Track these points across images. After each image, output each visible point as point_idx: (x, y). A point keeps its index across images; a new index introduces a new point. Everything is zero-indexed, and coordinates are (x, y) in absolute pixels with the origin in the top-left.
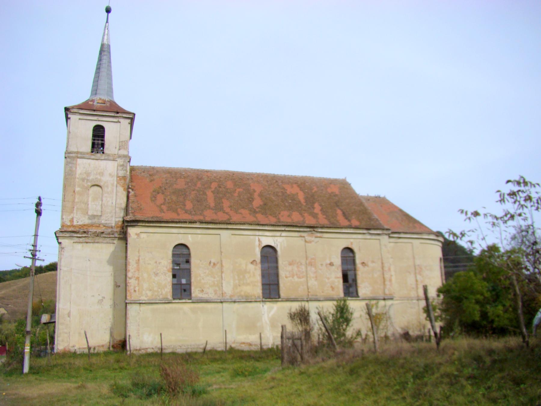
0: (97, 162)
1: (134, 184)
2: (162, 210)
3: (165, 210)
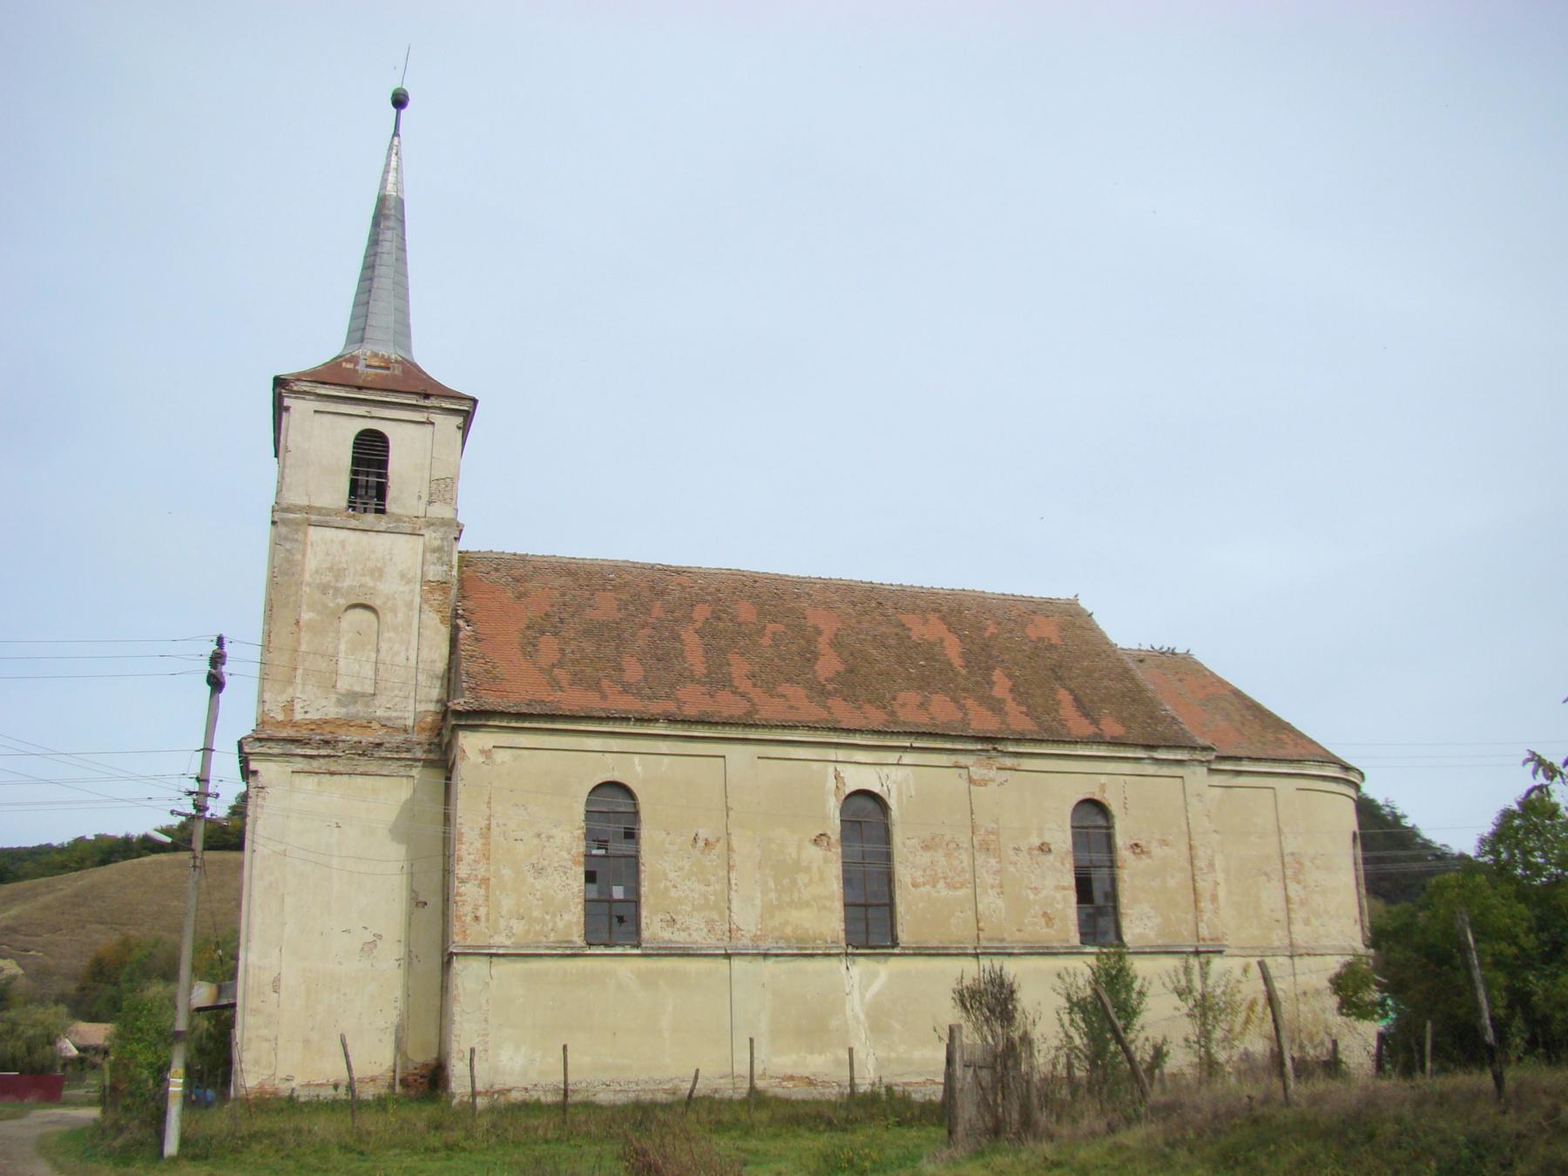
0: (364, 537)
1: (470, 604)
2: (555, 684)
3: (564, 683)
